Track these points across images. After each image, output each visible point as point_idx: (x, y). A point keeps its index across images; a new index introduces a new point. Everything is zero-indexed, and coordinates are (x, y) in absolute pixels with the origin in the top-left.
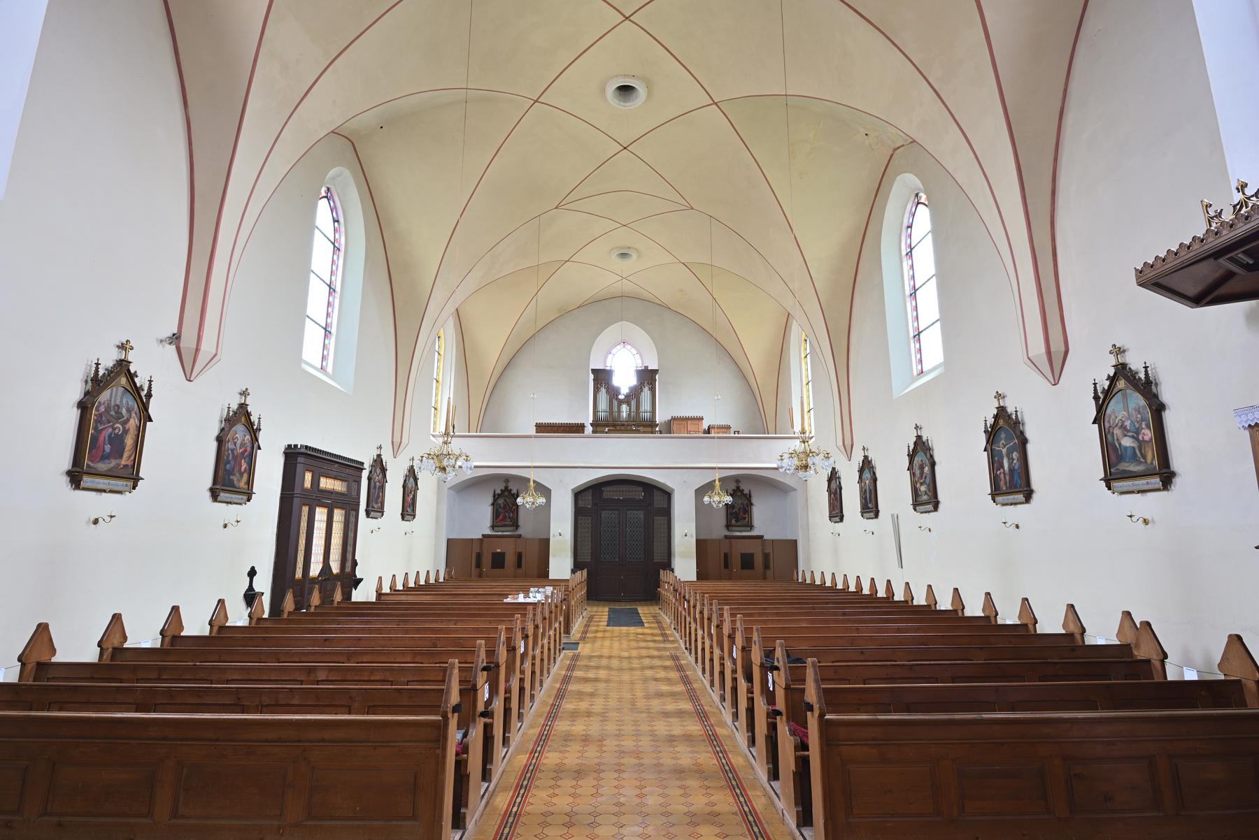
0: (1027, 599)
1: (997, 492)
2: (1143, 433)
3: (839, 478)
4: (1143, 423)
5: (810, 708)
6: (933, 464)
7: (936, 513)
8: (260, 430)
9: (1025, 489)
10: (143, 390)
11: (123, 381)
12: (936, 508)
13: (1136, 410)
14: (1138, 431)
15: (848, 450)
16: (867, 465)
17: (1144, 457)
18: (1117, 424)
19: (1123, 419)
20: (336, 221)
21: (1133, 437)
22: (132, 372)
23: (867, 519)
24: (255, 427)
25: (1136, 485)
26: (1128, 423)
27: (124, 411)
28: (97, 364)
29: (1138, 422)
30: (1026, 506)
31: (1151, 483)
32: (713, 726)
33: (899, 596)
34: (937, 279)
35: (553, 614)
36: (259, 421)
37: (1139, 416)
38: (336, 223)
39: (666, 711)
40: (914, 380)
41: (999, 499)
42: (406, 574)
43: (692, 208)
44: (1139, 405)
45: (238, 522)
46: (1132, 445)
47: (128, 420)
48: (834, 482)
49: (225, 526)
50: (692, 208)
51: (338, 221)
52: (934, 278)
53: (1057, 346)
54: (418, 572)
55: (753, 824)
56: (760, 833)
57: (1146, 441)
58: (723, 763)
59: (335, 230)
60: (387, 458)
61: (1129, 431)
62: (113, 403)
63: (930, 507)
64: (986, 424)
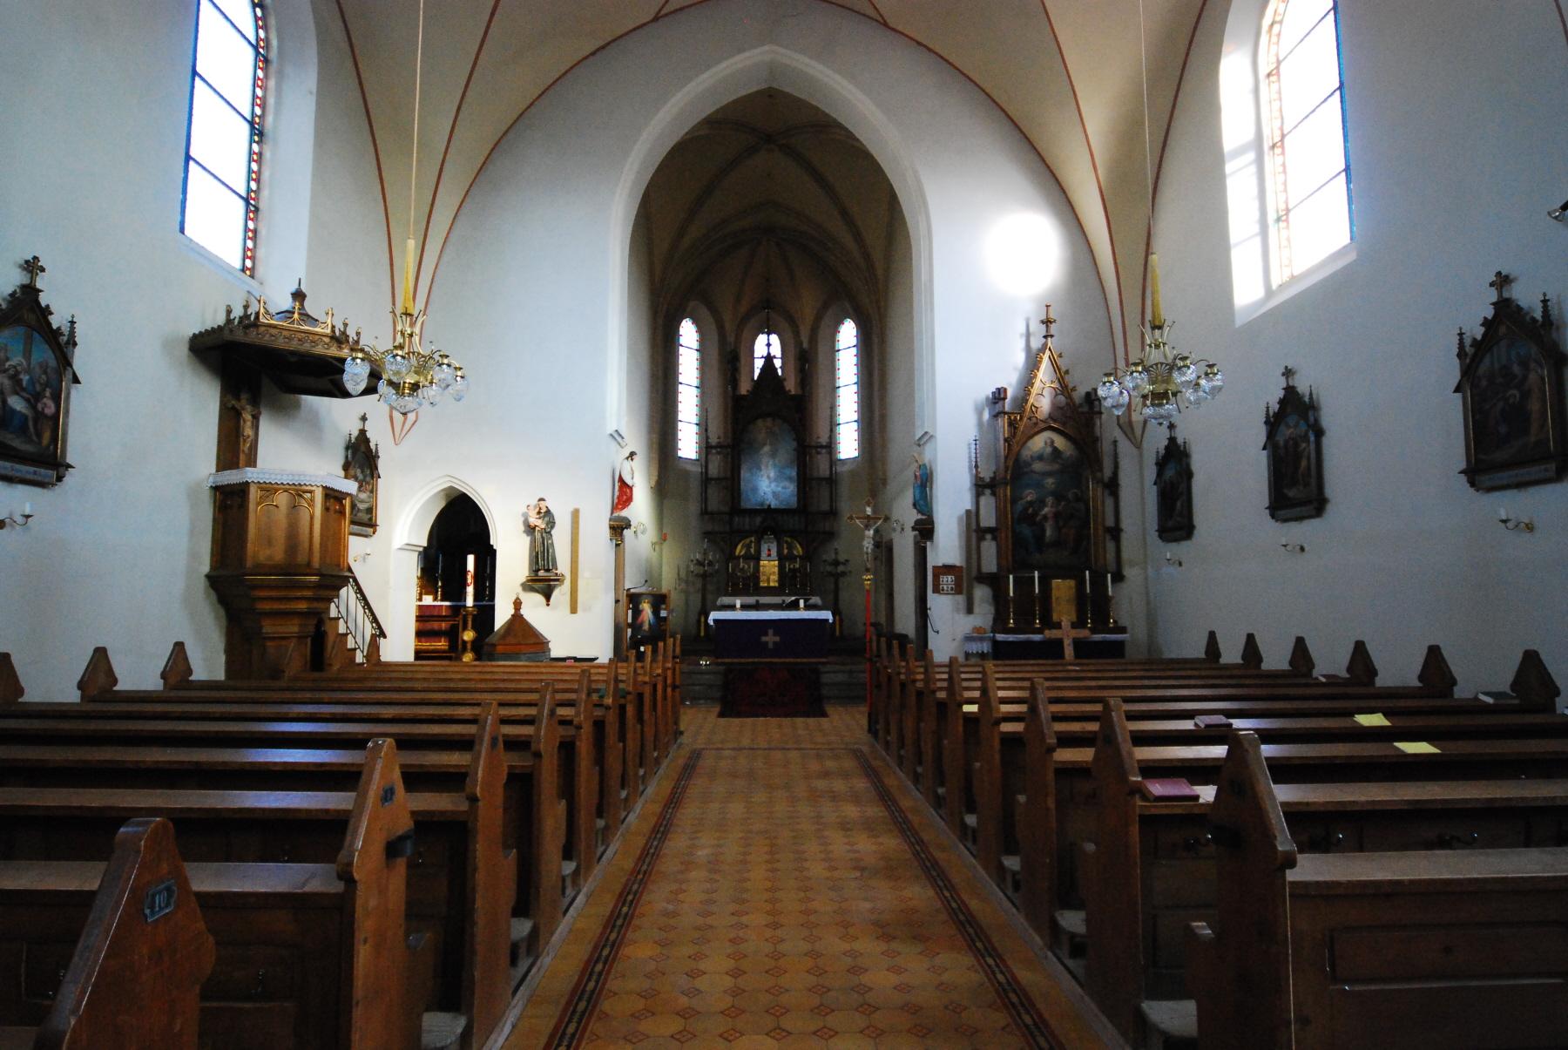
2: (45, 404)
4: (48, 389)
5: (757, 601)
13: (41, 367)
14: (38, 397)
17: (39, 435)
18: (8, 370)
19: (19, 368)
21: (28, 400)
22: (43, 304)
25: (18, 471)
26: (25, 378)
27: (1516, 369)
29: (41, 384)
31: (40, 475)
37: (44, 377)
44: (47, 363)
46: (24, 411)
47: (1525, 378)
57: (46, 416)
61: (24, 389)
62: (1497, 366)
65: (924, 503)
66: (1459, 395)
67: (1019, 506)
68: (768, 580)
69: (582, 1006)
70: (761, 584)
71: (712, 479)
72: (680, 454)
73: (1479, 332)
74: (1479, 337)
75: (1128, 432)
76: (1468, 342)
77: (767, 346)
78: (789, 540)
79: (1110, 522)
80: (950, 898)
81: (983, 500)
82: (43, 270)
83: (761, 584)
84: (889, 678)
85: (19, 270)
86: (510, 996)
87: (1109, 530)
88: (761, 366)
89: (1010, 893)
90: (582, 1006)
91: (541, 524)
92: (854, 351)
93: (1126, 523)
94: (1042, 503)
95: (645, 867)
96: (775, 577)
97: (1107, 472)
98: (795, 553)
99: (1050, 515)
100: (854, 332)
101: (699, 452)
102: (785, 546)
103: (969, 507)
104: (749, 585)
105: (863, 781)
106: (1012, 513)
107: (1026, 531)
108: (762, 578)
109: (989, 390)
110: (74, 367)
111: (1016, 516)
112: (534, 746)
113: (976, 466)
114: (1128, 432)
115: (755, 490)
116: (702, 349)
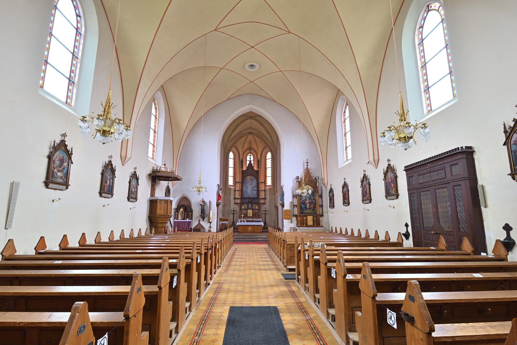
0: (387, 232)
1: (387, 195)
3: (333, 191)
6: (370, 185)
7: (397, 200)
8: (72, 154)
9: (396, 194)
10: (69, 152)
11: (63, 148)
12: (370, 202)
15: (376, 163)
16: (345, 186)
20: (78, 15)
22: (66, 144)
23: (345, 206)
24: (70, 153)
28: (54, 142)
30: (370, 204)
32: (312, 320)
33: (372, 236)
34: (350, 132)
35: (275, 191)
36: (72, 150)
38: (78, 18)
39: (278, 287)
40: (345, 163)
41: (388, 198)
42: (132, 229)
43: (290, 32)
45: (109, 205)
48: (331, 193)
49: (53, 201)
50: (290, 32)
51: (80, 16)
52: (349, 132)
53: (376, 158)
54: (140, 229)
55: (317, 334)
56: (317, 333)
58: (299, 305)
59: (78, 22)
60: (116, 163)
63: (368, 201)
64: (384, 170)
65: (282, 199)
66: (505, 147)
67: (301, 201)
68: (250, 215)
69: (203, 322)
70: (248, 216)
71: (236, 190)
72: (229, 184)
73: (512, 124)
74: (512, 126)
75: (324, 185)
76: (507, 127)
77: (250, 158)
78: (255, 205)
79: (320, 204)
80: (302, 309)
81: (294, 199)
82: (67, 136)
83: (248, 216)
84: (299, 252)
85: (60, 136)
86: (185, 320)
87: (320, 206)
88: (248, 163)
89: (330, 321)
90: (203, 322)
91: (203, 204)
92: (271, 159)
93: (324, 204)
94: (306, 200)
95: (212, 302)
96: (252, 214)
97: (320, 194)
98: (256, 208)
99: (308, 202)
100: (271, 155)
101: (233, 184)
102: (254, 206)
103: (291, 201)
104: (246, 216)
105: (292, 299)
106: (300, 202)
107: (303, 206)
108: (248, 214)
109: (295, 176)
110: (72, 159)
111: (301, 203)
112: (178, 267)
113: (293, 192)
114: (324, 185)
115: (247, 193)
116: (234, 159)
